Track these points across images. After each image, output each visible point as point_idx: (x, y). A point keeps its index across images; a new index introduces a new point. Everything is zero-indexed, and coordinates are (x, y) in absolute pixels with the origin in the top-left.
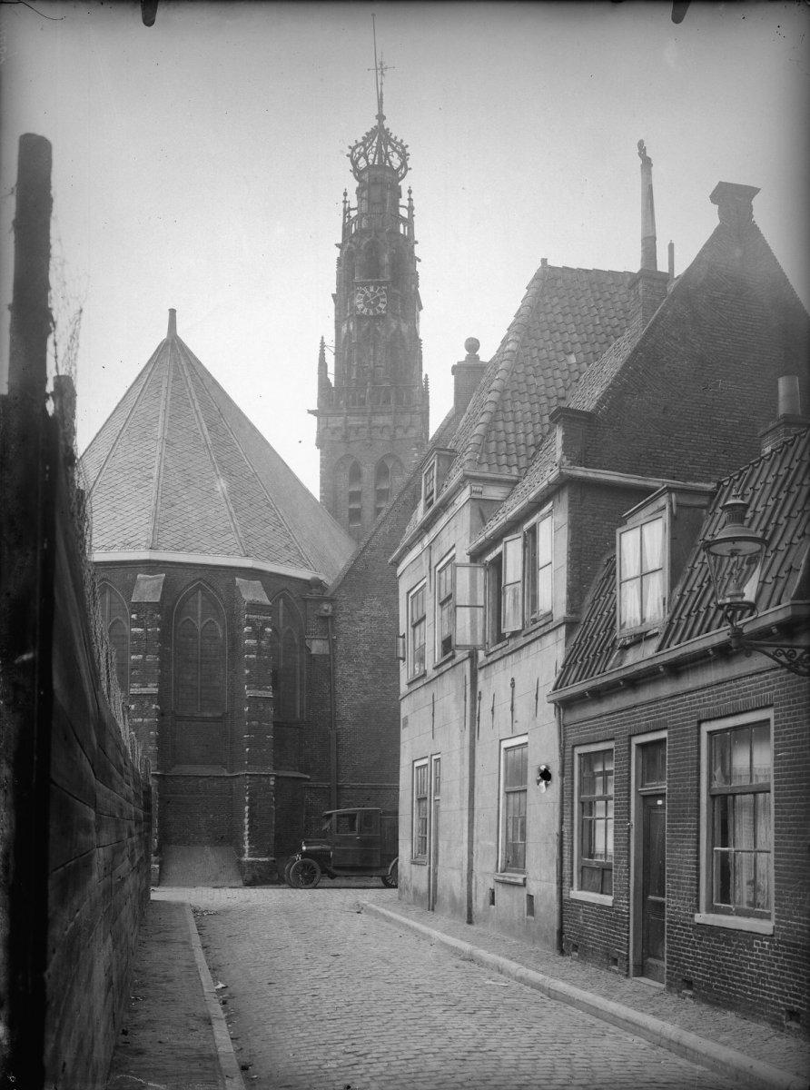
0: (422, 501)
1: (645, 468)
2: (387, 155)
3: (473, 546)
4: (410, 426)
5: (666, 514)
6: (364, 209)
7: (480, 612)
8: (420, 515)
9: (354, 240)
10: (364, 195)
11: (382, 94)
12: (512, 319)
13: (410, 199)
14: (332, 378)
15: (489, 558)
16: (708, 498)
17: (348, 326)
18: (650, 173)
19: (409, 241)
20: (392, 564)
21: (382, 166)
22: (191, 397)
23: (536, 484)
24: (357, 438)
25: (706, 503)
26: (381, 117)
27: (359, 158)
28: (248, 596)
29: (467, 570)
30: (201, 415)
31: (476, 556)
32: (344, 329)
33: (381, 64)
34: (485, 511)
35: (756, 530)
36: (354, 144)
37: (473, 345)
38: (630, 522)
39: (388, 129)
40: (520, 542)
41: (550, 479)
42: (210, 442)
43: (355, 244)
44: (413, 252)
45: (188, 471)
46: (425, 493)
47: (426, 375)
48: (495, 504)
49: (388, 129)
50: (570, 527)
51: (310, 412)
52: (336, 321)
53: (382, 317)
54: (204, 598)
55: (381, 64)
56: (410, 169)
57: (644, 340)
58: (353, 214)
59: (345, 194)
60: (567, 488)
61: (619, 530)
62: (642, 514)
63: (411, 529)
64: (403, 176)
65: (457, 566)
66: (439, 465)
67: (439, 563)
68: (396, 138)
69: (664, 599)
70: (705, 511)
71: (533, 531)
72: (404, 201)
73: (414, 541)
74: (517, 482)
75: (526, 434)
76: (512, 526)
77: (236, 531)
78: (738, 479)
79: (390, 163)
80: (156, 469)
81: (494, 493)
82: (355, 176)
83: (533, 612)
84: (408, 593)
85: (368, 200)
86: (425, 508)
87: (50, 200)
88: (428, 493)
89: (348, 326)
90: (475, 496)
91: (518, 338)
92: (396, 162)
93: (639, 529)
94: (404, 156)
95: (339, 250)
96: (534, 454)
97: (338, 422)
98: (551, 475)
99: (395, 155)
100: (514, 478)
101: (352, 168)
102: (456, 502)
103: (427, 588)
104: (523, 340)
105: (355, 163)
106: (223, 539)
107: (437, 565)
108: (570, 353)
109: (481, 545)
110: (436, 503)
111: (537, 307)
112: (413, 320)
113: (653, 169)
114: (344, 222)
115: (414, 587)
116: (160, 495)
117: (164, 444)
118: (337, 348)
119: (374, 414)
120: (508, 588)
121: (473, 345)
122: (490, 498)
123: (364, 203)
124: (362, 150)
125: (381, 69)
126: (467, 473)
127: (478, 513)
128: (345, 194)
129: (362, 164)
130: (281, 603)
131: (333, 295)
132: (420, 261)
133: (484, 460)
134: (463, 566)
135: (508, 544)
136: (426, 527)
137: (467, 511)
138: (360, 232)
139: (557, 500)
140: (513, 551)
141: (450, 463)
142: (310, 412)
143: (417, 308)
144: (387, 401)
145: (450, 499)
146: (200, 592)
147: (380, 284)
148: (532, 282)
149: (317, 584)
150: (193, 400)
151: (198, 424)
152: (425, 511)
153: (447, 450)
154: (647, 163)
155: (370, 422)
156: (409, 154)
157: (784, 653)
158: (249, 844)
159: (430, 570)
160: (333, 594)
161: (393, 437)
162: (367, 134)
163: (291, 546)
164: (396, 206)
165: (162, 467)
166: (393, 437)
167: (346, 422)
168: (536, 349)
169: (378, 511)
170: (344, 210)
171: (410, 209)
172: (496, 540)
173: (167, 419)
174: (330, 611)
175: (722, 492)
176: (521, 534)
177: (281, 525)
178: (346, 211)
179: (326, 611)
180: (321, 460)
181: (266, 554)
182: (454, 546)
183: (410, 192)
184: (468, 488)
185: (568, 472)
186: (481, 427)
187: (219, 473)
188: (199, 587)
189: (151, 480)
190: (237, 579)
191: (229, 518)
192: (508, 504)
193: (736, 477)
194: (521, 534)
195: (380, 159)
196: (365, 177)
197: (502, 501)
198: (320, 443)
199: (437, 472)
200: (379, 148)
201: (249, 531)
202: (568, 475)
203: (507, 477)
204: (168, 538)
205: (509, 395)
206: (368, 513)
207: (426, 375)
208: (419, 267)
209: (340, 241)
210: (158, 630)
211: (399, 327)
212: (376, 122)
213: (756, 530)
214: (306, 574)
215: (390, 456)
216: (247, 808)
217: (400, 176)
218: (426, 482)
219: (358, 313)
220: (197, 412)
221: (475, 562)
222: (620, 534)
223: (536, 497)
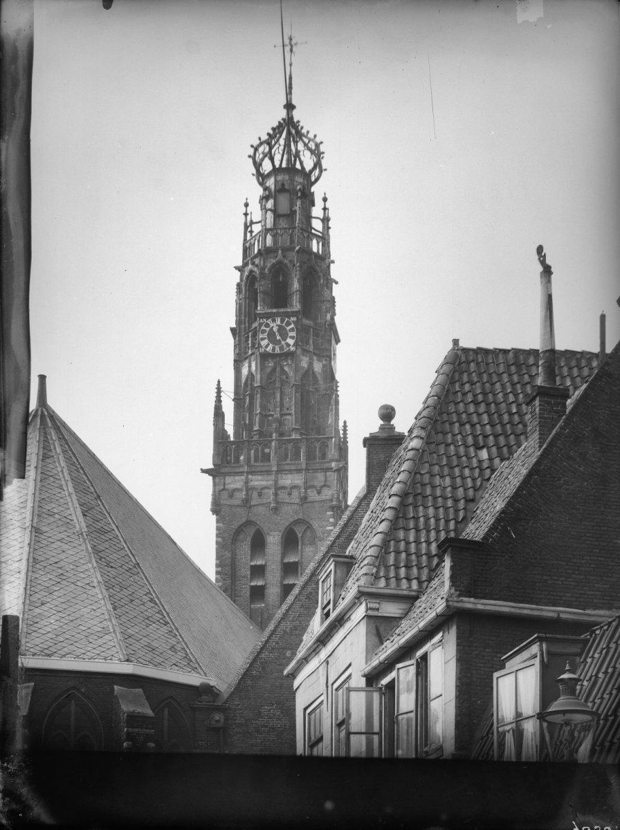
0: (319, 611)
1: (540, 596)
2: (297, 155)
3: (369, 668)
4: (325, 486)
5: (537, 661)
6: (269, 224)
7: (376, 738)
8: (316, 626)
9: (257, 261)
10: (270, 204)
11: (291, 78)
12: (420, 407)
13: (325, 209)
14: (229, 428)
15: (385, 681)
16: (581, 646)
17: (250, 367)
18: (549, 281)
19: (324, 259)
20: (288, 676)
21: (291, 170)
22: (64, 477)
23: (429, 610)
24: (261, 501)
25: (579, 650)
26: (290, 107)
27: (262, 160)
28: (126, 707)
29: (363, 694)
30: (74, 497)
31: (372, 678)
32: (245, 371)
33: (291, 39)
34: (382, 629)
35: (586, 701)
36: (256, 143)
37: (387, 414)
38: (508, 665)
39: (298, 122)
40: (413, 670)
41: (438, 611)
43: (257, 266)
44: (329, 274)
45: (62, 564)
46: (322, 604)
47: (345, 422)
48: (392, 622)
49: (298, 122)
50: (458, 660)
52: (235, 361)
53: (290, 355)
55: (291, 39)
56: (326, 170)
57: (538, 463)
58: (257, 228)
59: (246, 205)
60: (455, 621)
61: (496, 675)
62: (518, 658)
63: (308, 639)
64: (317, 180)
65: (349, 690)
66: (335, 572)
67: (337, 680)
68: (308, 132)
69: (537, 746)
70: (578, 658)
71: (425, 658)
72: (317, 211)
73: (309, 655)
74: (417, 598)
75: (429, 543)
76: (405, 652)
77: (114, 631)
78: (607, 630)
79: (301, 163)
81: (391, 609)
82: (258, 180)
83: (426, 745)
84: (305, 709)
85: (274, 211)
86: (322, 618)
88: (325, 602)
89: (250, 367)
90: (370, 613)
91: (423, 434)
92: (308, 161)
93: (514, 674)
94: (317, 153)
95: (239, 273)
96: (438, 565)
98: (440, 606)
99: (308, 153)
100: (414, 593)
101: (254, 171)
102: (352, 617)
103: (324, 706)
104: (429, 436)
105: (257, 165)
106: (100, 641)
107: (335, 682)
108: (482, 448)
109: (375, 668)
110: (333, 616)
111: (447, 396)
112: (327, 355)
113: (553, 276)
114: (245, 239)
115: (313, 702)
116: (28, 592)
117: (34, 534)
118: (236, 393)
119: (279, 471)
120: (400, 717)
121: (387, 414)
122: (388, 615)
123: (270, 215)
124: (267, 149)
125: (289, 46)
126: (361, 589)
127: (375, 632)
128: (246, 205)
129: (267, 167)
130: (166, 712)
131: (232, 330)
132: (337, 283)
133: (382, 574)
134: (358, 690)
135: (401, 671)
136: (323, 640)
137: (363, 628)
138: (265, 252)
139: (446, 630)
140: (405, 674)
141: (348, 572)
143: (333, 342)
144: (297, 455)
145: (345, 614)
147: (288, 315)
148: (442, 366)
149: (207, 690)
150: (66, 481)
151: (72, 509)
152: (322, 623)
153: (346, 557)
154: (547, 271)
155: (276, 481)
156: (323, 153)
159: (327, 687)
160: (226, 702)
161: (304, 499)
162: (274, 129)
163: (178, 647)
164: (309, 218)
165: (31, 560)
166: (304, 499)
168: (443, 446)
169: (287, 589)
170: (246, 224)
171: (326, 220)
172: (387, 666)
173: (36, 504)
174: (222, 721)
175: (594, 641)
176: (413, 661)
177: (166, 623)
178: (247, 227)
179: (217, 721)
181: (149, 656)
182: (350, 665)
183: (325, 200)
184: (364, 605)
185: (456, 604)
186: (384, 524)
187: (95, 565)
190: (116, 687)
191: (107, 617)
192: (404, 623)
193: (606, 628)
194: (413, 661)
195: (289, 160)
196: (271, 183)
197: (401, 618)
199: (335, 581)
200: (287, 145)
201: (129, 631)
202: (455, 607)
203: (405, 593)
204: (38, 641)
205: (411, 500)
206: (273, 592)
207: (345, 422)
208: (336, 291)
209: (240, 263)
211: (311, 364)
212: (283, 114)
213: (586, 701)
214: (194, 679)
215: (298, 522)
217: (313, 179)
218: (323, 589)
219: (262, 350)
220: (70, 495)
221: (372, 686)
222: (497, 678)
223: (426, 627)
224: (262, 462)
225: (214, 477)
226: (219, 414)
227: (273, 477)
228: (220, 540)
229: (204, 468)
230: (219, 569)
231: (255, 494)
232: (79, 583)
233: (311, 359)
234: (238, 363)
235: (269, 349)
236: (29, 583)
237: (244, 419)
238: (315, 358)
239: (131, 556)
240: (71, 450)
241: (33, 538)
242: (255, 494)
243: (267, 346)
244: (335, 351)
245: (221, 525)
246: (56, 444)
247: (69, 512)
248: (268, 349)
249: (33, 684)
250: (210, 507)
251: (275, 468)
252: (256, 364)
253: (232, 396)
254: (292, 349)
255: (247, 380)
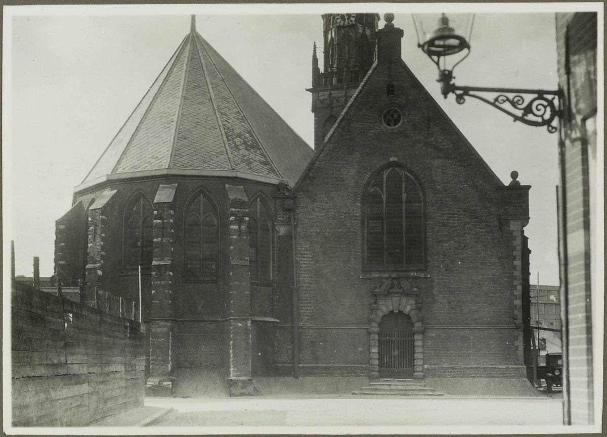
14: (322, 70)
17: (332, 34)
42: (213, 97)
51: (307, 90)
52: (324, 32)
54: (205, 199)
77: (227, 153)
80: (176, 115)
87: (529, 264)
89: (332, 34)
97: (324, 95)
118: (325, 48)
142: (307, 90)
146: (202, 195)
155: (346, 93)
157: (508, 99)
158: (233, 367)
165: (180, 114)
167: (330, 94)
180: (315, 120)
188: (202, 191)
189: (172, 123)
190: (226, 185)
198: (315, 109)
210: (171, 220)
211: (364, 31)
214: (274, 180)
216: (232, 342)
224: (561, 385)
225: (313, 93)
226: (315, 60)
227: (344, 91)
228: (316, 126)
229: (308, 88)
230: (317, 142)
231: (335, 102)
232: (207, 127)
233: (364, 28)
234: (326, 33)
235: (342, 24)
236: (178, 127)
237: (329, 62)
238: (366, 28)
239: (241, 112)
240: (208, 55)
241: (182, 102)
242: (335, 102)
243: (340, 23)
244: (377, 24)
245: (317, 118)
246: (199, 52)
247: (204, 87)
248: (341, 24)
249: (177, 184)
250: (311, 109)
251: (345, 87)
252: (335, 32)
253: (323, 50)
254: (354, 23)
255: (330, 42)
